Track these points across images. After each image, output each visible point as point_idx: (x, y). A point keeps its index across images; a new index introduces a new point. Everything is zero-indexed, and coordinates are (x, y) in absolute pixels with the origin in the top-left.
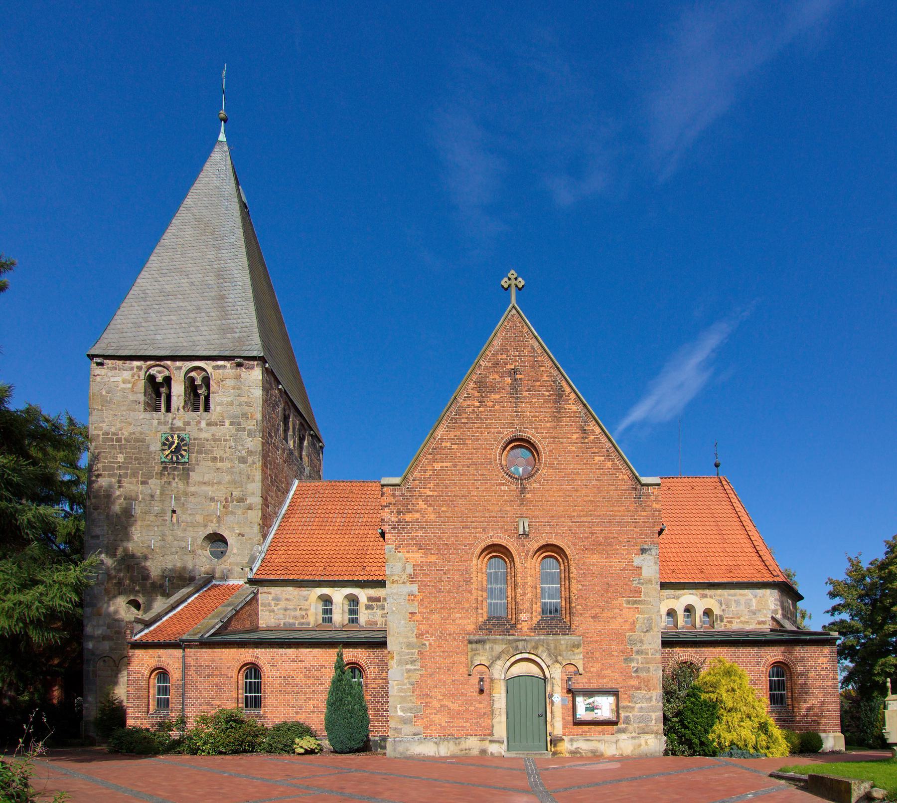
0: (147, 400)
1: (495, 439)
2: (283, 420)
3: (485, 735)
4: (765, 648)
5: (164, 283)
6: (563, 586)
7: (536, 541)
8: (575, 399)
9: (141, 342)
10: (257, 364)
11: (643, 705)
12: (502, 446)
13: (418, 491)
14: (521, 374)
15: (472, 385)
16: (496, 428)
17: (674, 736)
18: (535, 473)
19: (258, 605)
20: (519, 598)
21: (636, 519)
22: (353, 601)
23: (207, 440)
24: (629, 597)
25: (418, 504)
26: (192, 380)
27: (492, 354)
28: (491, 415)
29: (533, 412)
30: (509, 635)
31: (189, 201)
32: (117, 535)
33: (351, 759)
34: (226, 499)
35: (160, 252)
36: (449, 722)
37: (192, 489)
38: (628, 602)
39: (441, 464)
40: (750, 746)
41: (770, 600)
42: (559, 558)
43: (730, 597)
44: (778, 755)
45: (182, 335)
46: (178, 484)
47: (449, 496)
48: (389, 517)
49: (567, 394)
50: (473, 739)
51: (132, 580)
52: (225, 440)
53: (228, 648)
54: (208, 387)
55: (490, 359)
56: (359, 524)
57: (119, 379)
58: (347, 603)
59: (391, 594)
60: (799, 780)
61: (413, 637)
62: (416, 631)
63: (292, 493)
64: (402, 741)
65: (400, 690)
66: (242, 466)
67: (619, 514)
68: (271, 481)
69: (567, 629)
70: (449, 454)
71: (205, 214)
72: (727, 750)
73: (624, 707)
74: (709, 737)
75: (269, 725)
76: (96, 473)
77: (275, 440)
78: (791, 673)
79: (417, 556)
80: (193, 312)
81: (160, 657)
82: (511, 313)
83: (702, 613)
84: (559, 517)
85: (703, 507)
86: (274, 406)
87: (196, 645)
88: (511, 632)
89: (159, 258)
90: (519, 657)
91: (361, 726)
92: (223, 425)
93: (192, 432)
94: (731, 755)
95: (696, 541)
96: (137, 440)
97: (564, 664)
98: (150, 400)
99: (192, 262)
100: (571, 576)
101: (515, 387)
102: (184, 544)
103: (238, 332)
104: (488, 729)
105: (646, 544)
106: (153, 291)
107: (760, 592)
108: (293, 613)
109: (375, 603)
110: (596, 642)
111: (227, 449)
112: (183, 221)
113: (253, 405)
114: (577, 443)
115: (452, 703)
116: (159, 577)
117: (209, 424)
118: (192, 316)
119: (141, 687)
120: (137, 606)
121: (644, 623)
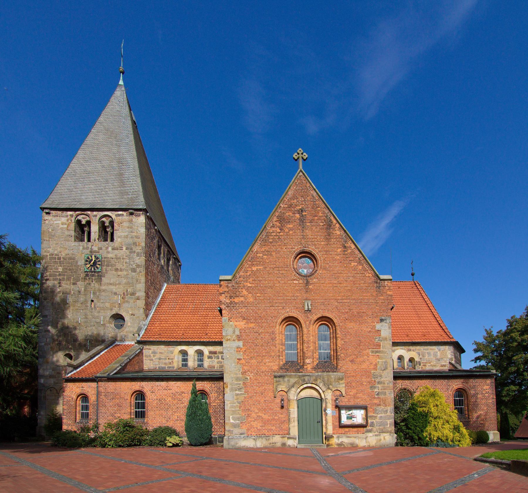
0: (76, 235)
1: (290, 252)
2: (158, 248)
3: (285, 434)
4: (452, 380)
5: (86, 166)
6: (332, 342)
7: (315, 314)
8: (339, 227)
9: (73, 200)
10: (142, 214)
11: (382, 415)
12: (294, 256)
14: (305, 212)
15: (275, 219)
16: (290, 245)
17: (401, 434)
18: (314, 273)
19: (143, 356)
20: (305, 349)
21: (377, 301)
22: (200, 353)
23: (112, 259)
24: (373, 349)
25: (243, 292)
26: (103, 223)
27: (288, 200)
28: (287, 237)
29: (313, 236)
30: (299, 372)
31: (101, 119)
32: (58, 315)
33: (202, 450)
34: (124, 293)
35: (84, 148)
36: (262, 426)
37: (103, 287)
38: (373, 352)
39: (256, 267)
40: (450, 440)
41: (448, 352)
42: (329, 325)
43: (424, 351)
44: (465, 446)
45: (97, 196)
46: (95, 285)
47: (262, 287)
48: (225, 300)
49: (334, 225)
50: (277, 436)
51: (67, 342)
52: (123, 259)
53: (125, 381)
54: (113, 227)
55: (286, 203)
56: (203, 309)
57: (60, 222)
58: (196, 355)
60: (502, 464)
61: (239, 374)
62: (241, 370)
63: (163, 291)
64: (234, 438)
65: (232, 407)
66: (133, 274)
67: (367, 298)
68: (151, 283)
69: (335, 369)
70: (261, 261)
71: (111, 126)
72: (435, 442)
73: (370, 417)
74: (424, 434)
75: (150, 428)
76: (46, 278)
77: (153, 259)
78: (467, 394)
79: (242, 324)
80: (104, 183)
81: (83, 388)
82: (299, 175)
83: (408, 360)
84: (330, 299)
85: (406, 299)
86: (153, 239)
87: (105, 380)
88: (301, 370)
89: (84, 152)
90: (305, 386)
91: (208, 429)
92: (122, 250)
93: (103, 254)
94: (437, 445)
95: (403, 318)
96: (70, 258)
98: (78, 235)
99: (103, 154)
100: (337, 336)
101: (302, 220)
102: (98, 320)
103: (131, 194)
104: (287, 430)
105: (383, 316)
106: (80, 171)
107: (442, 348)
108: (164, 361)
109: (213, 355)
110: (353, 376)
111: (124, 264)
112: (98, 130)
113: (140, 237)
114: (340, 254)
115: (264, 414)
116: (84, 340)
117: (113, 249)
118: (104, 185)
119: (71, 406)
120: (70, 357)
121: (382, 365)
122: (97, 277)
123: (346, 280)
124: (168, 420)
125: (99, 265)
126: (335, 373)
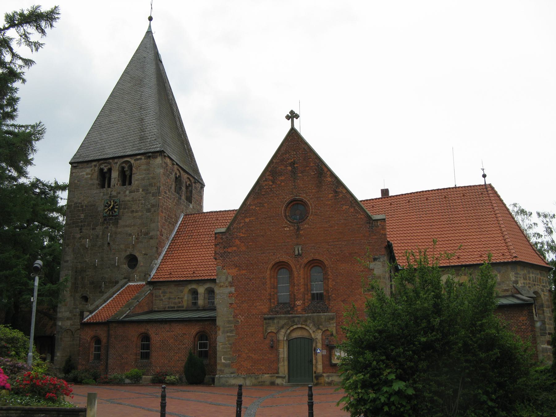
7: (306, 258)
13: (236, 235)
14: (297, 164)
21: (370, 241)
25: (236, 242)
30: (289, 314)
34: (138, 234)
37: (119, 230)
46: (112, 228)
47: (254, 236)
52: (139, 200)
59: (219, 293)
63: (179, 222)
66: (148, 214)
67: (359, 238)
79: (234, 271)
90: (295, 327)
97: (324, 330)
101: (294, 172)
111: (140, 205)
115: (254, 354)
122: (114, 221)
123: (337, 223)
124: (170, 361)
125: (117, 208)
126: (326, 314)
